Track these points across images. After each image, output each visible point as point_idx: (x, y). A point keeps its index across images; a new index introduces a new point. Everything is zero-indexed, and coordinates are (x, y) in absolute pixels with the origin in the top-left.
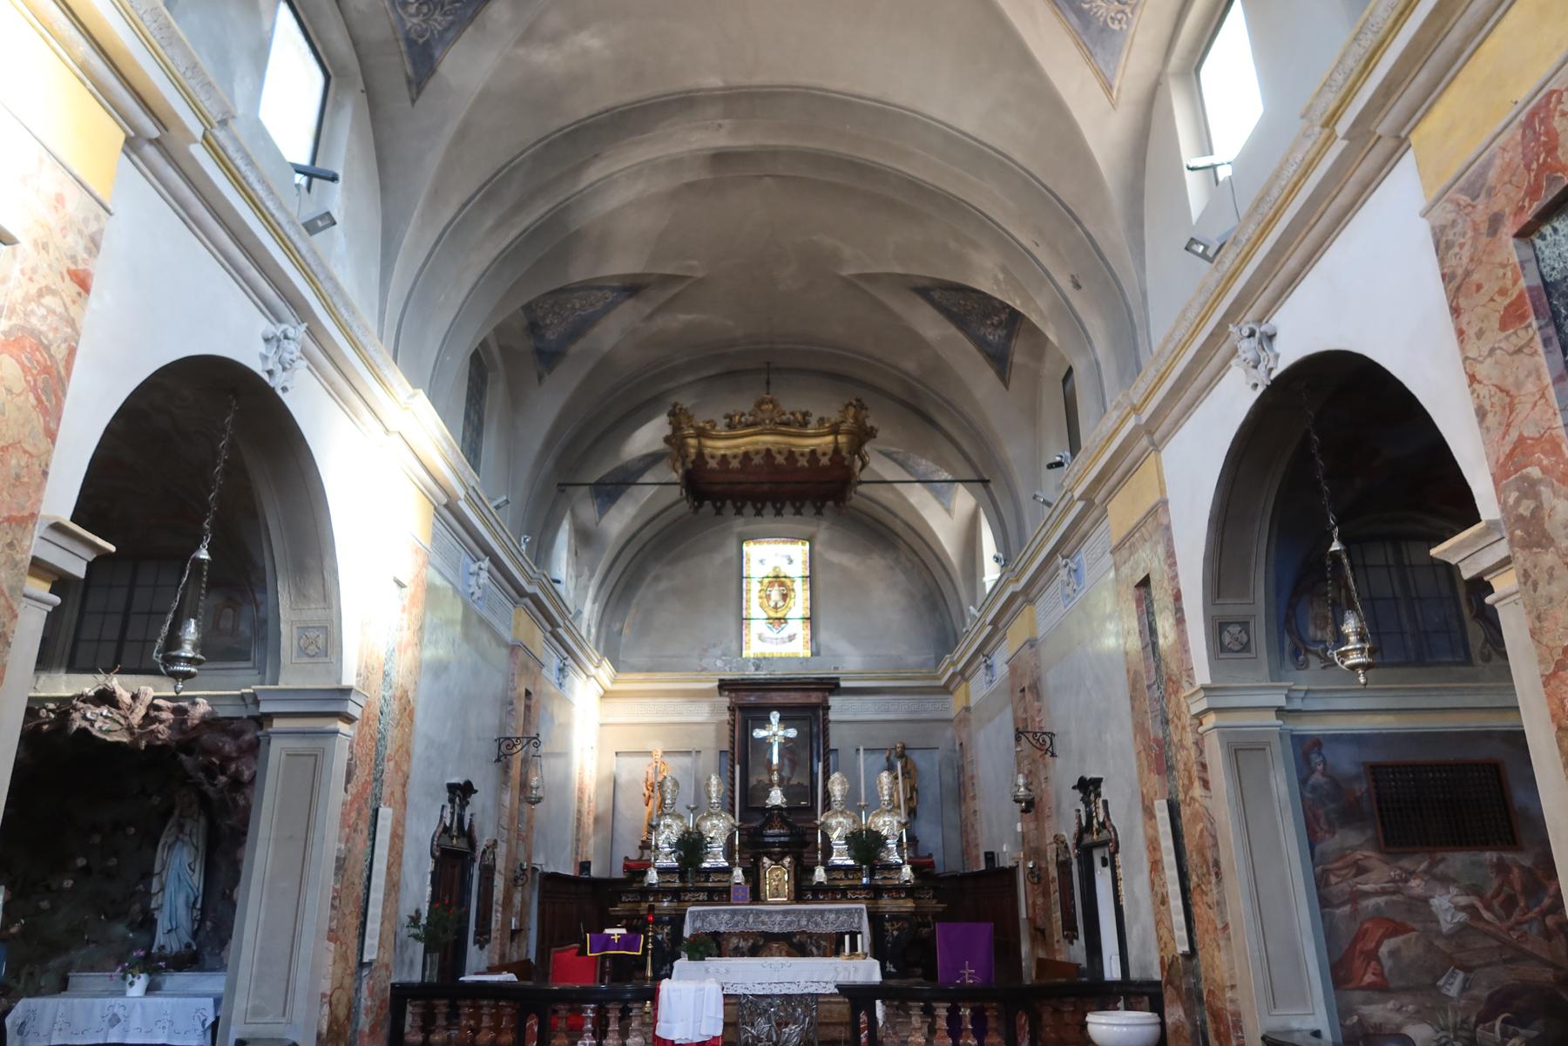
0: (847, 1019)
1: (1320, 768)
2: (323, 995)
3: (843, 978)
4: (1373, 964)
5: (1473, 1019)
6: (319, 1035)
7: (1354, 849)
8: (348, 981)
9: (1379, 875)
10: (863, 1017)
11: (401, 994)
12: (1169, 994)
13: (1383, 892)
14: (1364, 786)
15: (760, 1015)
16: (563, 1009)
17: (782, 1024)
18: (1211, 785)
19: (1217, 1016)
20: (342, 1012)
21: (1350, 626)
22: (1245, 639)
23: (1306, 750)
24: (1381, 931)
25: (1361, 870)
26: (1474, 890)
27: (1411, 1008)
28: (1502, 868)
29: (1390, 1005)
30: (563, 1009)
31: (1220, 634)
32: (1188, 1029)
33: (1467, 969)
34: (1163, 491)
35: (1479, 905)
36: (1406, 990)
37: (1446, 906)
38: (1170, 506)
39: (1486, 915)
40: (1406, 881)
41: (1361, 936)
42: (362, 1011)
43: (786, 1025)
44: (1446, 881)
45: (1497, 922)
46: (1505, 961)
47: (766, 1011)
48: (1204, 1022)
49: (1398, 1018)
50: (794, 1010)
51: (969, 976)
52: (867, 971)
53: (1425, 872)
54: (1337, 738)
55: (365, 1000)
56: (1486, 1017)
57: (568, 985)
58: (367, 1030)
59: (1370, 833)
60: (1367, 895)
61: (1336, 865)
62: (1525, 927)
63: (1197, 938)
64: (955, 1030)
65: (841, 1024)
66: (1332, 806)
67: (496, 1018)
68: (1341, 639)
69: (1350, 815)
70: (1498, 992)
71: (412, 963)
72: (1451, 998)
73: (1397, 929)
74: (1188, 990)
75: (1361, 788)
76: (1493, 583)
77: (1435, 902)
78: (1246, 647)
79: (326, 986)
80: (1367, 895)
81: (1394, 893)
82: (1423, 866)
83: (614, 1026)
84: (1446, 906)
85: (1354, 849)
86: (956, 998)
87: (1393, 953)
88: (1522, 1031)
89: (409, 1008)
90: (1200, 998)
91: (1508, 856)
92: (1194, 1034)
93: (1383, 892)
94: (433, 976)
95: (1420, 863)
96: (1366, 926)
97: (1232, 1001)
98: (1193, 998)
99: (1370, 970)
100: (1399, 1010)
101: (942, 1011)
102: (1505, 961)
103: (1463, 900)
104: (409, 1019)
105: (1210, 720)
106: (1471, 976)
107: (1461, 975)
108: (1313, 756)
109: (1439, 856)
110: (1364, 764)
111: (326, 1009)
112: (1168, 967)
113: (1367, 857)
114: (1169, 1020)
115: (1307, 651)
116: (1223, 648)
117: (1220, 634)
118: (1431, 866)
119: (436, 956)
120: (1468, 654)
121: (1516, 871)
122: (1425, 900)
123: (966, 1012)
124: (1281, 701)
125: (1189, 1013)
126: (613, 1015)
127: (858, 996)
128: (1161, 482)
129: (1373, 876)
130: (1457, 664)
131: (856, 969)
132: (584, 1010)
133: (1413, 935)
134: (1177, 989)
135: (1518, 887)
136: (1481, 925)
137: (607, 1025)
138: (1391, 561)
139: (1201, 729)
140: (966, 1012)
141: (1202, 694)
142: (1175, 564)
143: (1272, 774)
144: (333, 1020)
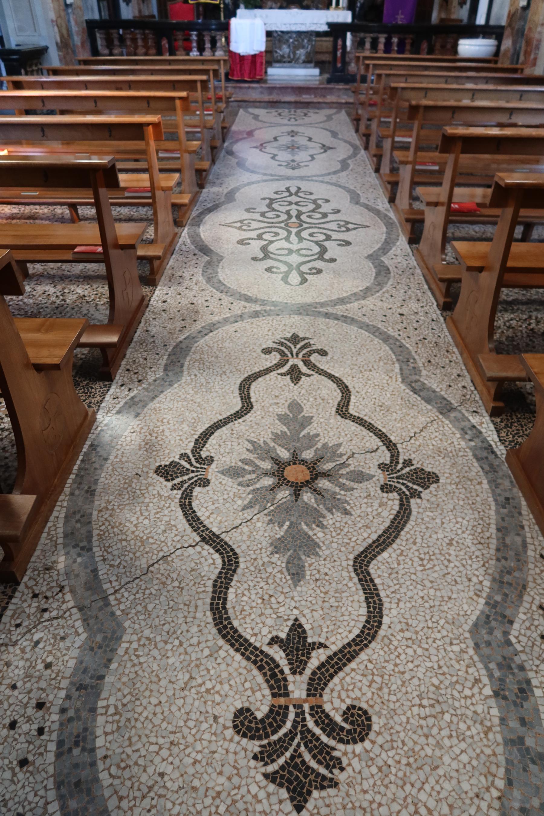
0: (331, 50)
2: (52, 21)
3: (331, 20)
6: (57, 44)
8: (63, 14)
10: (340, 42)
11: (92, 27)
12: (507, 32)
15: (284, 43)
16: (180, 35)
17: (296, 48)
19: (528, 43)
20: (65, 32)
30: (180, 35)
32: (512, 51)
42: (74, 34)
43: (298, 50)
47: (288, 41)
48: (520, 48)
50: (303, 40)
51: (401, 19)
52: (346, 17)
55: (75, 29)
57: (180, 21)
58: (79, 44)
64: (388, 48)
65: (327, 53)
67: (145, 40)
71: (92, 9)
74: (518, 30)
79: (52, 15)
83: (208, 45)
86: (391, 31)
89: (98, 35)
90: (523, 34)
92: (513, 55)
94: (105, 15)
97: (540, 33)
98: (520, 34)
101: (382, 40)
104: (99, 42)
111: (56, 29)
112: (512, 17)
114: (503, 48)
119: (105, 3)
123: (395, 40)
125: (514, 43)
126: (207, 39)
127: (336, 30)
131: (338, 16)
132: (191, 35)
134: (512, 29)
137: (204, 44)
140: (395, 40)
142: (525, 690)
144: (62, 36)
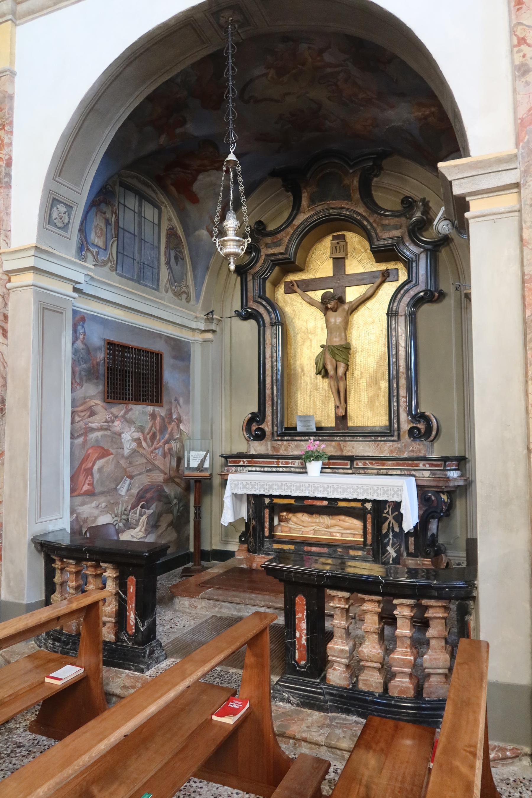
1: (81, 337)
4: (90, 477)
5: (129, 507)
7: (91, 398)
9: (103, 414)
13: (101, 429)
14: (102, 355)
18: (9, 334)
21: (231, 223)
22: (66, 221)
23: (80, 320)
24: (96, 455)
25: (93, 414)
26: (141, 429)
27: (103, 505)
28: (153, 416)
29: (94, 504)
31: (52, 208)
33: (131, 477)
34: (12, 62)
35: (142, 438)
36: (102, 493)
37: (128, 437)
38: (17, 79)
39: (144, 444)
40: (113, 422)
41: (86, 458)
44: (130, 422)
45: (147, 449)
46: (148, 471)
49: (96, 512)
53: (123, 416)
54: (95, 318)
56: (134, 507)
59: (101, 388)
60: (92, 430)
61: (81, 408)
62: (157, 451)
63: (523, 403)
66: (84, 366)
68: (222, 233)
69: (91, 374)
70: (142, 489)
72: (122, 496)
73: (105, 453)
75: (101, 356)
76: (471, 204)
77: (124, 436)
78: (65, 227)
80: (92, 430)
81: (106, 429)
82: (122, 413)
84: (128, 437)
85: (91, 398)
87: (100, 470)
88: (147, 511)
91: (157, 409)
93: (101, 429)
95: (121, 410)
96: (90, 451)
99: (87, 482)
100: (97, 507)
102: (148, 471)
103: (137, 435)
105: (29, 278)
106: (132, 481)
107: (128, 480)
108: (79, 327)
109: (130, 406)
110: (105, 340)
113: (97, 404)
115: (88, 249)
116: (50, 221)
117: (52, 208)
118: (126, 413)
120: (158, 285)
121: (158, 418)
122: (120, 435)
124: (80, 278)
128: (12, 54)
129: (97, 417)
130: (153, 289)
133: (111, 457)
135: (158, 428)
136: (141, 450)
138: (137, 211)
139: (9, 285)
141: (32, 252)
143: (64, 334)
